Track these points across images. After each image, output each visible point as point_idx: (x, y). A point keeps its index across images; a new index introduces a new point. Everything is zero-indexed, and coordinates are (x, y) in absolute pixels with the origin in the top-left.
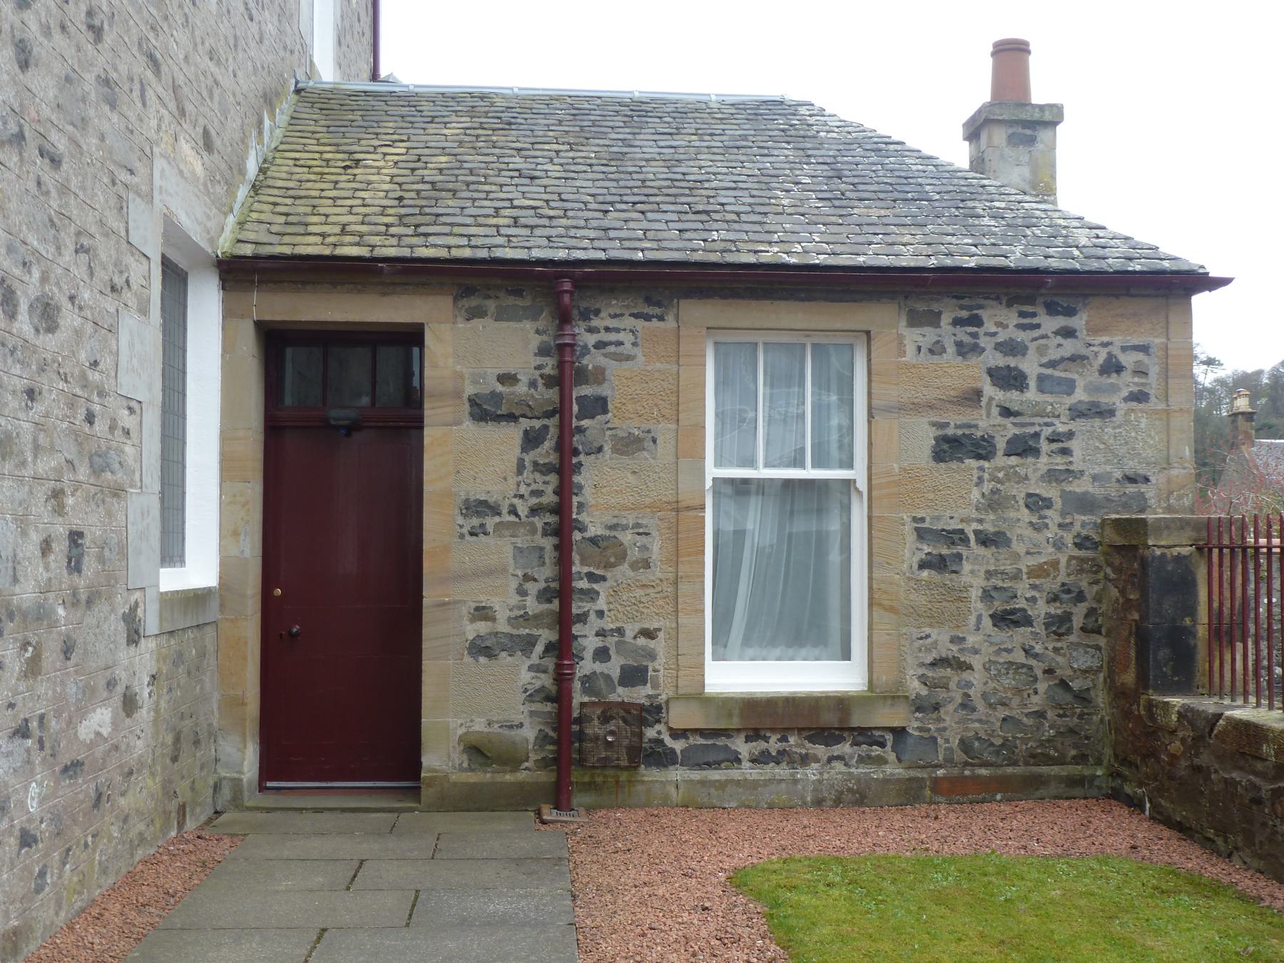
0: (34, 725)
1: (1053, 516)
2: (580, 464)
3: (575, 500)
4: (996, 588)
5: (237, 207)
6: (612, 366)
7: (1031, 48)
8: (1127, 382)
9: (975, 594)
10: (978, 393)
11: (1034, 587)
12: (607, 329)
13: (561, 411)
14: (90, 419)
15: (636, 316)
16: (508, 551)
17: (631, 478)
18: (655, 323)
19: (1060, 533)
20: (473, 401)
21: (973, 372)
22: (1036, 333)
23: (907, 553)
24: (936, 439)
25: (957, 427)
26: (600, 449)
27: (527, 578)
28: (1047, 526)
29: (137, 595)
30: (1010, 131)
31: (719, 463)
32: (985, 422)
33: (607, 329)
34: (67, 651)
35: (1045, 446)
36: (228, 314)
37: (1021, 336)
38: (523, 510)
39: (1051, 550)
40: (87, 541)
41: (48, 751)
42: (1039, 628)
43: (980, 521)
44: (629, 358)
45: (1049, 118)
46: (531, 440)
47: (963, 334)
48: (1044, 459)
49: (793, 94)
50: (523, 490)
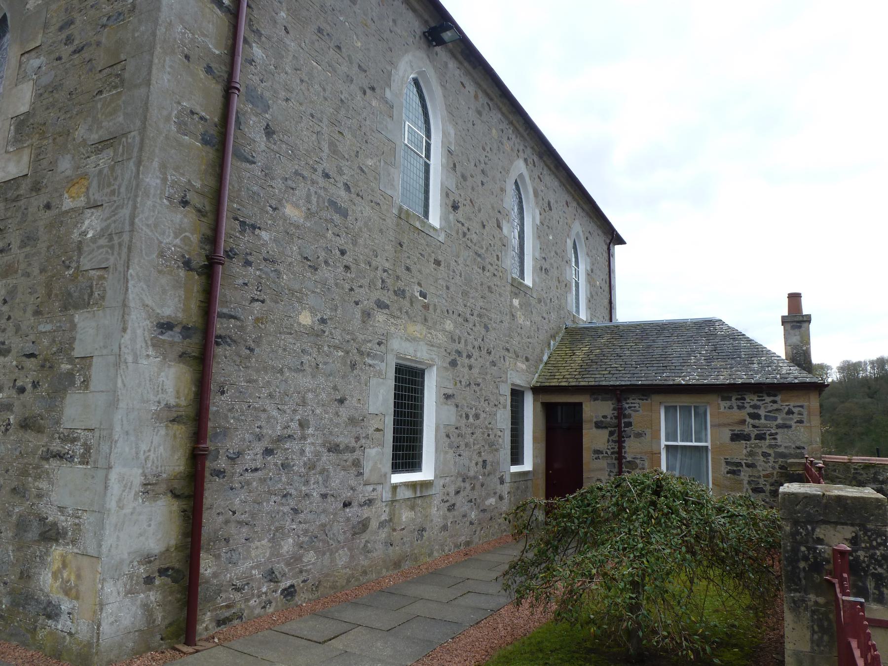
0: (473, 500)
1: (771, 459)
2: (625, 440)
3: (623, 450)
4: (752, 481)
5: (539, 371)
7: (802, 295)
8: (796, 417)
9: (745, 482)
10: (745, 421)
11: (765, 481)
12: (632, 403)
13: (619, 426)
14: (489, 435)
15: (639, 399)
16: (605, 465)
17: (639, 445)
18: (645, 401)
19: (774, 464)
20: (596, 423)
22: (764, 402)
23: (723, 469)
24: (732, 434)
25: (738, 431)
26: (630, 436)
27: (611, 472)
28: (769, 462)
29: (503, 473)
30: (792, 324)
31: (667, 440)
32: (747, 429)
33: (632, 403)
34: (482, 485)
35: (768, 437)
36: (534, 401)
37: (759, 403)
38: (609, 453)
39: (771, 469)
40: (488, 462)
41: (477, 506)
42: (768, 494)
43: (747, 460)
44: (638, 411)
45: (808, 319)
46: (611, 434)
47: (739, 403)
48: (767, 441)
49: (718, 317)
50: (609, 447)
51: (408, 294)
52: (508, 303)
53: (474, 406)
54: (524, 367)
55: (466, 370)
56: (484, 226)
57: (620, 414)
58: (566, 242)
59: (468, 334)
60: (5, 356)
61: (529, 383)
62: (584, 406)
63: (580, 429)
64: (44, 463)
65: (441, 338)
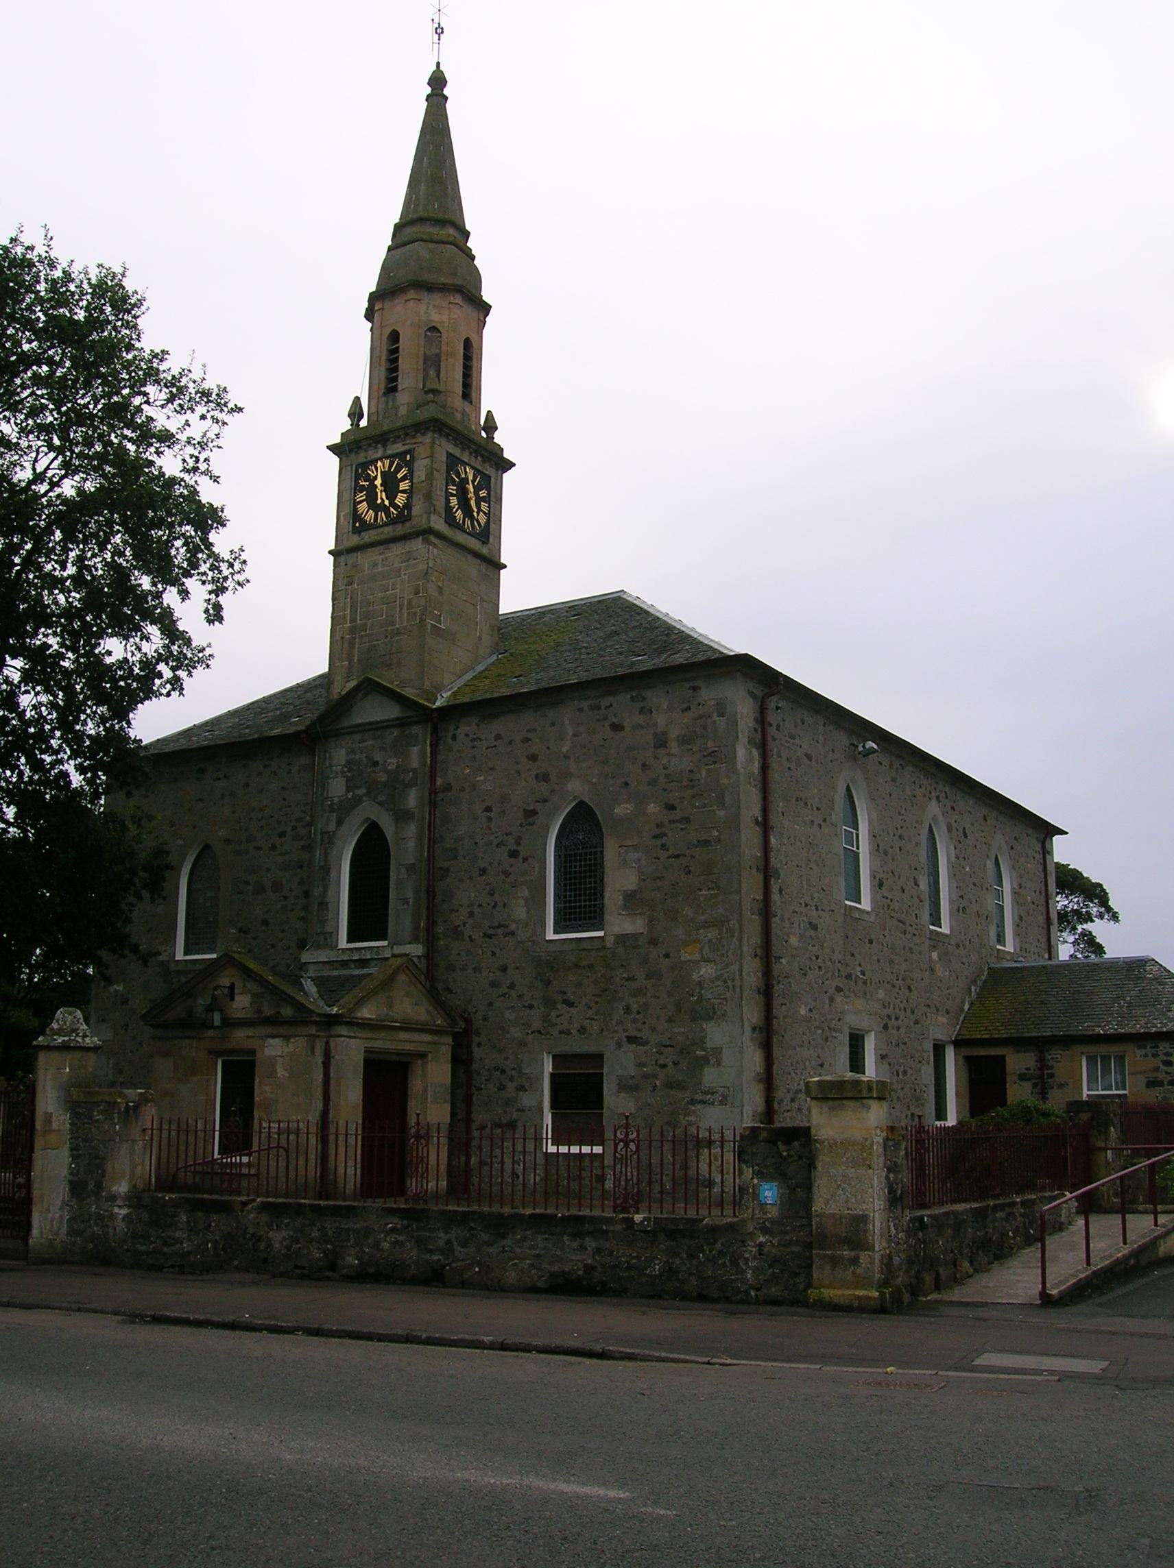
6: (1056, 1065)
13: (1041, 1077)
14: (915, 1090)
20: (1019, 1075)
21: (1157, 1062)
32: (1161, 1076)
36: (955, 1054)
44: (1060, 1062)
46: (1035, 1085)
47: (1153, 1050)
51: (854, 976)
52: (927, 958)
53: (902, 1063)
54: (945, 1020)
55: (895, 1031)
56: (903, 891)
57: (1043, 1064)
58: (985, 866)
59: (896, 998)
60: (644, 1046)
61: (950, 1037)
62: (1007, 1059)
63: (1004, 1082)
64: (690, 1106)
65: (876, 1006)
